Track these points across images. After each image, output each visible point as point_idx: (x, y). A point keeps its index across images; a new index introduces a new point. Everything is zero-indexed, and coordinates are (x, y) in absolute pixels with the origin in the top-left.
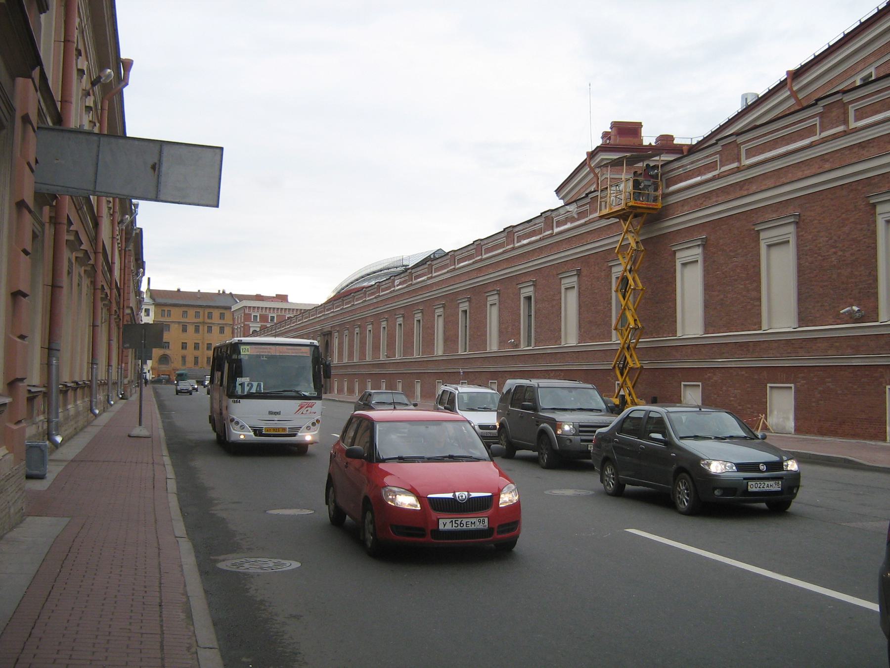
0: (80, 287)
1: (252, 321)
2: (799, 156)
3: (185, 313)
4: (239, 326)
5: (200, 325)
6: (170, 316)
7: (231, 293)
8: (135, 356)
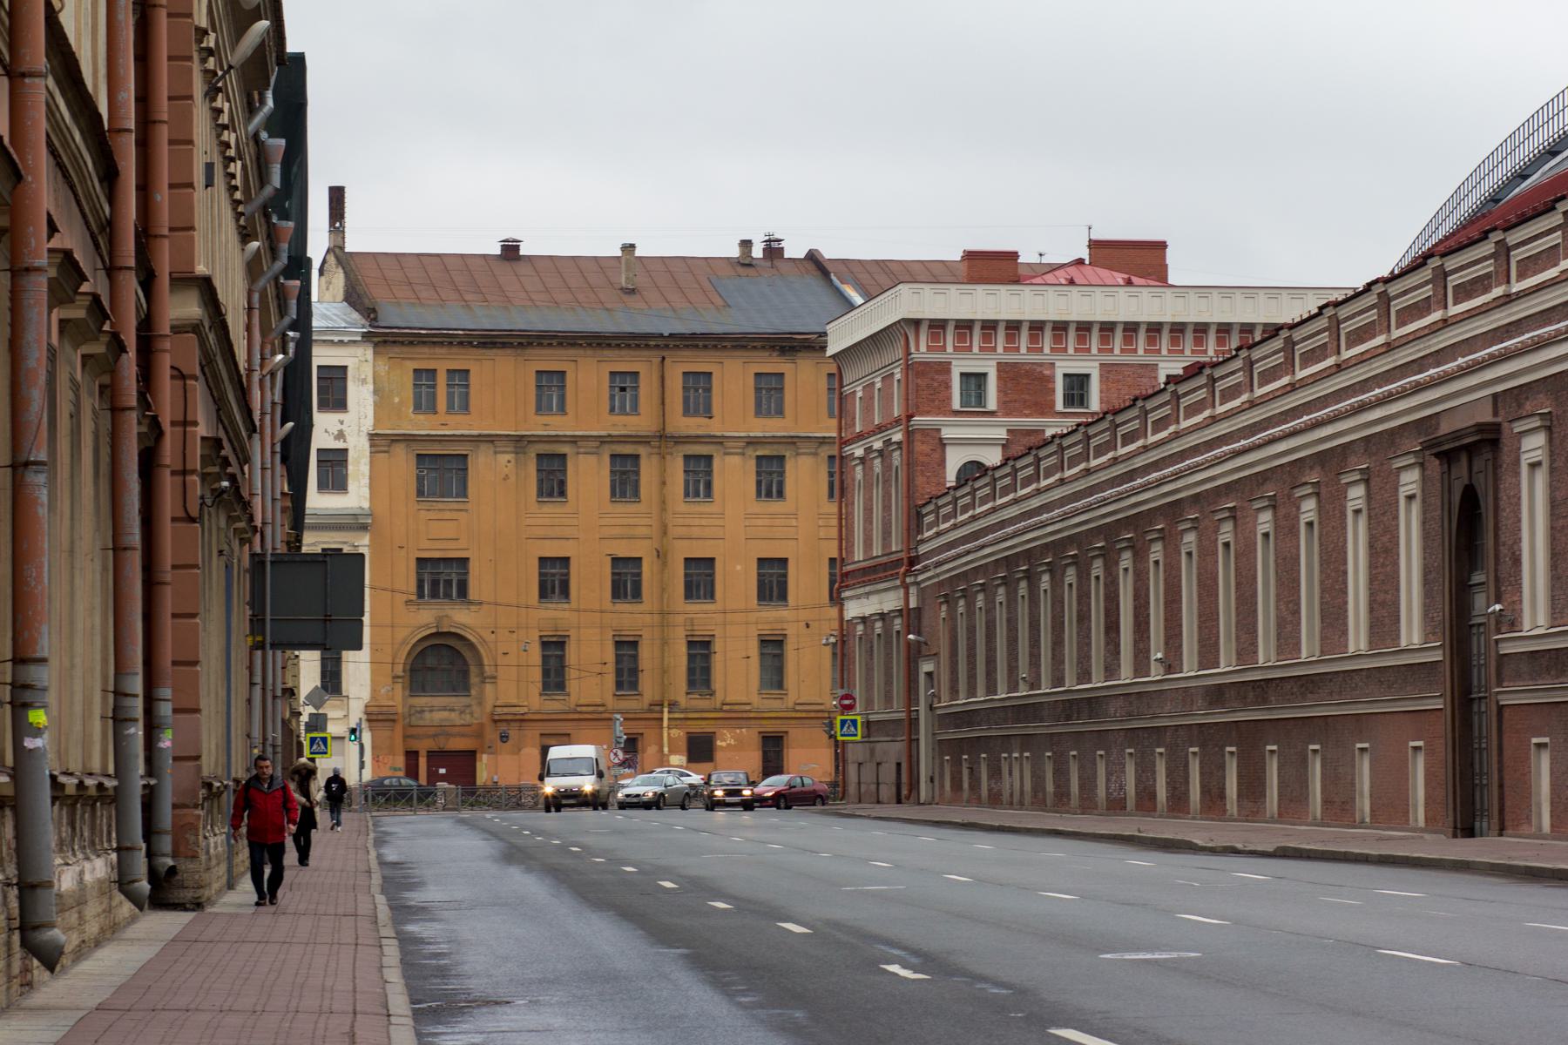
0: (74, 419)
1: (956, 405)
2: (1293, 398)
3: (551, 385)
4: (878, 445)
5: (642, 450)
6: (465, 407)
7: (813, 257)
8: (257, 623)
